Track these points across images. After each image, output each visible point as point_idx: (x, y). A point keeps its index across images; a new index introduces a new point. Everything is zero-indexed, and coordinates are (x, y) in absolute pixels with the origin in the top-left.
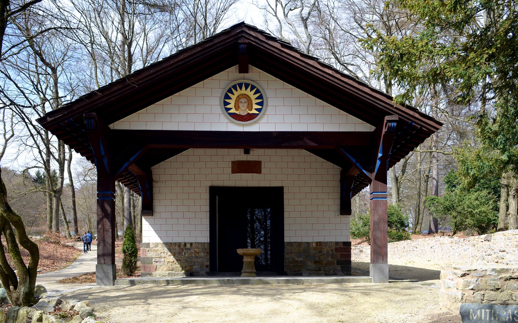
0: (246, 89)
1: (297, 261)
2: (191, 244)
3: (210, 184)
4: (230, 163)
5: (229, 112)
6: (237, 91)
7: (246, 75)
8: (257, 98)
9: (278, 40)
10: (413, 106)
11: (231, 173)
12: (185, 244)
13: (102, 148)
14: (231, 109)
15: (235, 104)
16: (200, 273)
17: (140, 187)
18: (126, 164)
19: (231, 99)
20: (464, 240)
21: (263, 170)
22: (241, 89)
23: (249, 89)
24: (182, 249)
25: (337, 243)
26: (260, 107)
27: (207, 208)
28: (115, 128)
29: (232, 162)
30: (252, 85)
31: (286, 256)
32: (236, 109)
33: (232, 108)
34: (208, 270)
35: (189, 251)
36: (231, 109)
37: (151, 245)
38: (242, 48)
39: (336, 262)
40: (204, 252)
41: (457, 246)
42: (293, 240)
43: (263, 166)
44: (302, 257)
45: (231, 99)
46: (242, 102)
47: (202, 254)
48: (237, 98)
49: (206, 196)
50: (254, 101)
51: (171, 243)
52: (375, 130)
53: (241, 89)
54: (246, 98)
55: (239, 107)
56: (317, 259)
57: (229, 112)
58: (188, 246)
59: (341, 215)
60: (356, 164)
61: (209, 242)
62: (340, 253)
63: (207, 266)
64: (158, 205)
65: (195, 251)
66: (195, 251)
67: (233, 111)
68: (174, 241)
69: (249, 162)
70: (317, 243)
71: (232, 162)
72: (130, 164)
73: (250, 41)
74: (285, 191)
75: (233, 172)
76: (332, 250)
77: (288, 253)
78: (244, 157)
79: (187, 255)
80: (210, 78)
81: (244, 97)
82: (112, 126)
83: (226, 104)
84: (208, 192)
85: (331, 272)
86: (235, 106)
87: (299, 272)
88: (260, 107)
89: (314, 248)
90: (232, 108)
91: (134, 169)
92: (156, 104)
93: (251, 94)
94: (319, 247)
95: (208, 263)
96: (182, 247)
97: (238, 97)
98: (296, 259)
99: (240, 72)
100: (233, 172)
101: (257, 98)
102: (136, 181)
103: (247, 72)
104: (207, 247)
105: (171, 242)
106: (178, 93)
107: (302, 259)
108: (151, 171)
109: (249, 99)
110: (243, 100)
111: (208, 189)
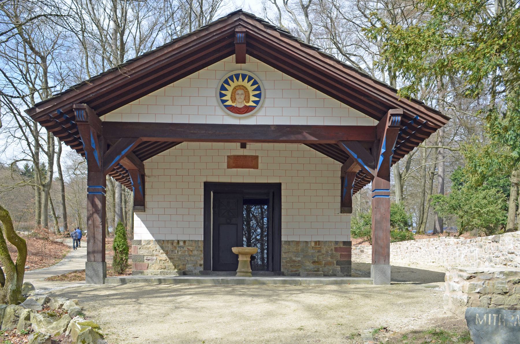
1: (294, 261)
2: (185, 242)
3: (205, 180)
4: (226, 158)
12: (178, 242)
13: (92, 140)
14: (227, 101)
16: (194, 272)
25: (337, 243)
29: (228, 156)
34: (202, 269)
37: (142, 242)
38: (239, 37)
41: (464, 247)
51: (163, 241)
54: (243, 89)
55: (235, 99)
58: (181, 244)
59: (342, 212)
62: (340, 253)
63: (201, 265)
65: (188, 249)
66: (188, 249)
67: (229, 103)
68: (167, 239)
72: (122, 158)
73: (248, 30)
82: (103, 118)
83: (222, 95)
86: (231, 98)
87: (297, 272)
88: (257, 99)
91: (126, 163)
94: (317, 246)
95: (202, 262)
96: (175, 244)
98: (294, 258)
99: (238, 62)
101: (254, 90)
102: (128, 176)
103: (244, 62)
106: (172, 84)
107: (299, 259)
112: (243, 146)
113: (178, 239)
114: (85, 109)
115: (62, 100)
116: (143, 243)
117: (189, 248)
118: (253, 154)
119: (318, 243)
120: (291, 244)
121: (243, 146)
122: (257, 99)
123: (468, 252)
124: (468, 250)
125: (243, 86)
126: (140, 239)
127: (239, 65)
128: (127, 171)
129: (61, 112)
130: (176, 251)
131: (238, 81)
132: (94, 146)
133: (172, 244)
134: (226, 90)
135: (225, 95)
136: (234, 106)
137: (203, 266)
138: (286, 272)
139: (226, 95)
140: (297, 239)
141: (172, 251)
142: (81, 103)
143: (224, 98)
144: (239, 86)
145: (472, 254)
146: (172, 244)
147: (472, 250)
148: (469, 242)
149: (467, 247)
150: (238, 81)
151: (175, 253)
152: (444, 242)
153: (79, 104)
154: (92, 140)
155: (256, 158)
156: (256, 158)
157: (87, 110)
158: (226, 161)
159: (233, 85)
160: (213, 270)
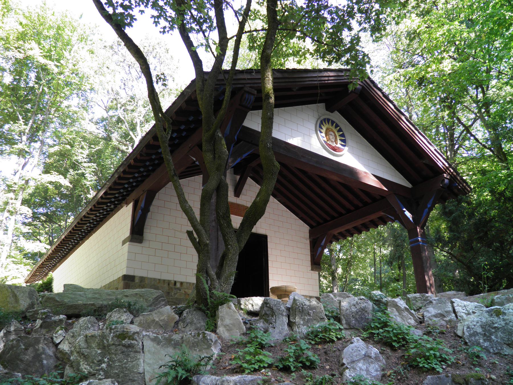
2: (182, 283)
12: (175, 283)
35: (178, 291)
51: (159, 280)
58: (178, 285)
59: (312, 270)
65: (185, 292)
66: (185, 292)
68: (163, 278)
80: (307, 106)
96: (171, 285)
105: (159, 278)
117: (186, 291)
130: (173, 294)
151: (172, 296)
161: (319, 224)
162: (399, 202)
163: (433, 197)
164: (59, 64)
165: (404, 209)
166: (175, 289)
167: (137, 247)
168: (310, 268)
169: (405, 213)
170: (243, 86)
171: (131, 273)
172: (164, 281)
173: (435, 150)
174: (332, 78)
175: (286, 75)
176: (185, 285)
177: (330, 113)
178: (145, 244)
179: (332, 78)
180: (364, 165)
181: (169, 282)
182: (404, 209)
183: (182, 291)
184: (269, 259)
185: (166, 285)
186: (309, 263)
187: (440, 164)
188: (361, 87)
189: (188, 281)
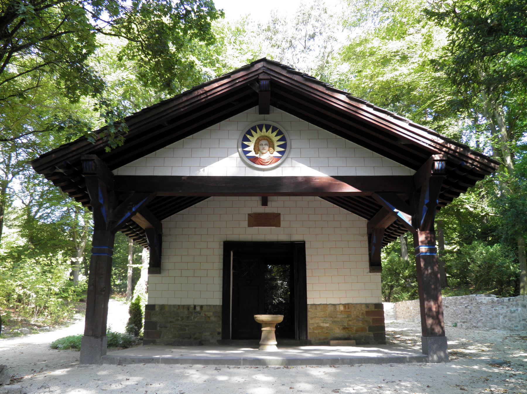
0: (267, 131)
1: (322, 328)
2: (202, 307)
3: (224, 238)
4: (247, 216)
5: (247, 155)
6: (256, 132)
7: (267, 116)
8: (279, 140)
9: (303, 75)
10: (464, 143)
11: (247, 226)
12: (195, 307)
13: (100, 195)
14: (250, 152)
15: (255, 146)
16: (211, 341)
17: (148, 242)
18: (128, 214)
19: (251, 141)
20: (509, 300)
21: (282, 223)
22: (261, 130)
23: (270, 131)
24: (191, 313)
25: (367, 305)
26: (282, 149)
27: (221, 266)
28: (119, 174)
29: (249, 215)
30: (273, 126)
31: (310, 321)
32: (255, 151)
33: (251, 151)
34: (219, 338)
35: (199, 315)
36: (250, 152)
37: (156, 307)
38: (263, 84)
39: (367, 328)
40: (215, 317)
41: (501, 306)
42: (317, 302)
43: (282, 219)
44: (328, 323)
45: (251, 141)
46: (262, 145)
47: (213, 319)
48: (256, 140)
49: (219, 251)
50: (276, 144)
51: (179, 306)
52: (416, 174)
53: (261, 130)
54: (267, 140)
55: (259, 150)
56: (346, 324)
57: (247, 155)
58: (198, 309)
59: (370, 272)
60: (425, 206)
61: (221, 304)
62: (372, 317)
63: (219, 333)
64: (167, 263)
65: (205, 315)
66: (205, 315)
67: (252, 154)
68: (183, 303)
69: (266, 215)
70: (345, 305)
71: (249, 215)
72: (134, 214)
73: (272, 78)
74: (307, 246)
75: (250, 225)
76: (362, 313)
77: (312, 318)
78: (262, 209)
79: (196, 320)
80: (227, 120)
81: (265, 139)
82: (117, 172)
83: (246, 139)
84: (222, 247)
85: (363, 340)
86: (254, 149)
87: (326, 341)
88: (282, 149)
89: (342, 311)
90: (251, 151)
91: (141, 221)
92: (166, 147)
93: (273, 136)
94: (347, 310)
95: (220, 330)
96: (191, 310)
97: (258, 139)
98: (322, 325)
99: (260, 113)
100: (250, 225)
101: (279, 140)
102: (145, 236)
103: (268, 113)
104: (219, 310)
105: (179, 304)
106: (191, 136)
107: (328, 325)
108: (161, 225)
109: (271, 141)
110: (263, 142)
111: (222, 243)
112: (265, 203)
113: (195, 304)
114: (93, 160)
115: (70, 151)
116: (157, 309)
117: (207, 313)
118: (275, 211)
119: (347, 307)
120: (318, 307)
121: (265, 203)
122: (282, 149)
123: (507, 312)
124: (508, 309)
125: (266, 136)
126: (154, 304)
127: (263, 115)
128: (144, 231)
129: (68, 164)
130: (192, 318)
131: (261, 131)
132: (101, 201)
133: (188, 310)
134: (249, 140)
135: (248, 146)
136: (257, 157)
137: (221, 334)
138: (313, 340)
139: (248, 146)
140: (323, 302)
141: (188, 317)
142: (90, 153)
143: (246, 149)
144: (263, 136)
145: (513, 315)
146: (188, 310)
147: (512, 310)
148: (507, 301)
149: (505, 307)
150: (261, 131)
151: (191, 320)
152: (475, 301)
153: (89, 155)
154: (100, 195)
155: (278, 216)
156: (278, 216)
157: (95, 161)
158: (247, 219)
159: (256, 136)
160: (233, 338)
161: (372, 217)
162: (385, 202)
163: (428, 189)
164: (216, 68)
165: (396, 210)
166: (195, 313)
167: (157, 277)
168: (368, 270)
169: (398, 214)
170: (80, 155)
171: (153, 303)
172: (184, 306)
173: (410, 125)
174: (241, 80)
175: (136, 120)
176: (205, 308)
177: (266, 116)
178: (164, 274)
179: (241, 80)
180: (319, 168)
181: (188, 307)
182: (396, 210)
183: (203, 314)
184: (307, 267)
185: (185, 311)
186: (367, 264)
187: (425, 143)
188: (267, 82)
189: (209, 303)
